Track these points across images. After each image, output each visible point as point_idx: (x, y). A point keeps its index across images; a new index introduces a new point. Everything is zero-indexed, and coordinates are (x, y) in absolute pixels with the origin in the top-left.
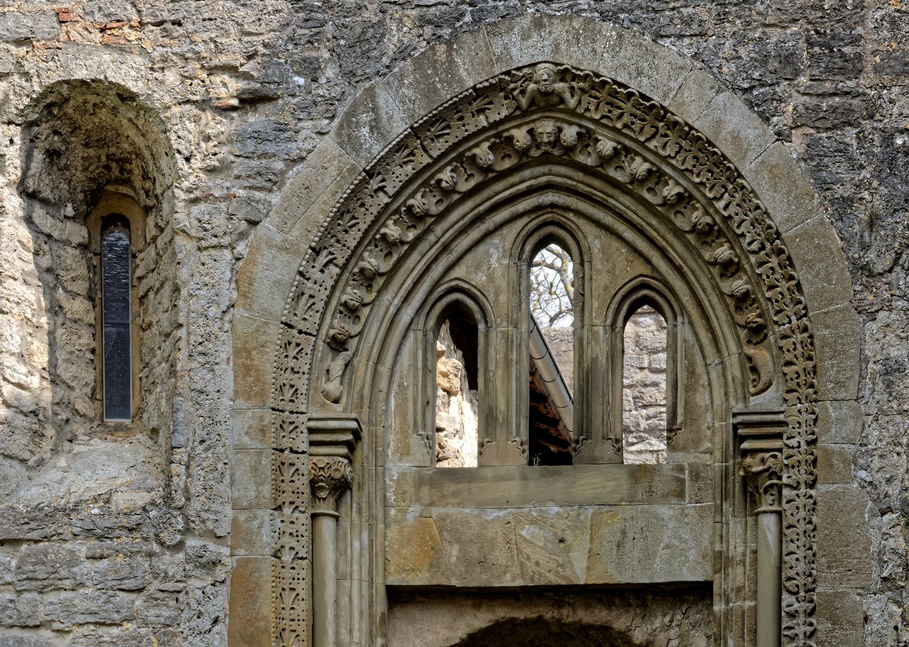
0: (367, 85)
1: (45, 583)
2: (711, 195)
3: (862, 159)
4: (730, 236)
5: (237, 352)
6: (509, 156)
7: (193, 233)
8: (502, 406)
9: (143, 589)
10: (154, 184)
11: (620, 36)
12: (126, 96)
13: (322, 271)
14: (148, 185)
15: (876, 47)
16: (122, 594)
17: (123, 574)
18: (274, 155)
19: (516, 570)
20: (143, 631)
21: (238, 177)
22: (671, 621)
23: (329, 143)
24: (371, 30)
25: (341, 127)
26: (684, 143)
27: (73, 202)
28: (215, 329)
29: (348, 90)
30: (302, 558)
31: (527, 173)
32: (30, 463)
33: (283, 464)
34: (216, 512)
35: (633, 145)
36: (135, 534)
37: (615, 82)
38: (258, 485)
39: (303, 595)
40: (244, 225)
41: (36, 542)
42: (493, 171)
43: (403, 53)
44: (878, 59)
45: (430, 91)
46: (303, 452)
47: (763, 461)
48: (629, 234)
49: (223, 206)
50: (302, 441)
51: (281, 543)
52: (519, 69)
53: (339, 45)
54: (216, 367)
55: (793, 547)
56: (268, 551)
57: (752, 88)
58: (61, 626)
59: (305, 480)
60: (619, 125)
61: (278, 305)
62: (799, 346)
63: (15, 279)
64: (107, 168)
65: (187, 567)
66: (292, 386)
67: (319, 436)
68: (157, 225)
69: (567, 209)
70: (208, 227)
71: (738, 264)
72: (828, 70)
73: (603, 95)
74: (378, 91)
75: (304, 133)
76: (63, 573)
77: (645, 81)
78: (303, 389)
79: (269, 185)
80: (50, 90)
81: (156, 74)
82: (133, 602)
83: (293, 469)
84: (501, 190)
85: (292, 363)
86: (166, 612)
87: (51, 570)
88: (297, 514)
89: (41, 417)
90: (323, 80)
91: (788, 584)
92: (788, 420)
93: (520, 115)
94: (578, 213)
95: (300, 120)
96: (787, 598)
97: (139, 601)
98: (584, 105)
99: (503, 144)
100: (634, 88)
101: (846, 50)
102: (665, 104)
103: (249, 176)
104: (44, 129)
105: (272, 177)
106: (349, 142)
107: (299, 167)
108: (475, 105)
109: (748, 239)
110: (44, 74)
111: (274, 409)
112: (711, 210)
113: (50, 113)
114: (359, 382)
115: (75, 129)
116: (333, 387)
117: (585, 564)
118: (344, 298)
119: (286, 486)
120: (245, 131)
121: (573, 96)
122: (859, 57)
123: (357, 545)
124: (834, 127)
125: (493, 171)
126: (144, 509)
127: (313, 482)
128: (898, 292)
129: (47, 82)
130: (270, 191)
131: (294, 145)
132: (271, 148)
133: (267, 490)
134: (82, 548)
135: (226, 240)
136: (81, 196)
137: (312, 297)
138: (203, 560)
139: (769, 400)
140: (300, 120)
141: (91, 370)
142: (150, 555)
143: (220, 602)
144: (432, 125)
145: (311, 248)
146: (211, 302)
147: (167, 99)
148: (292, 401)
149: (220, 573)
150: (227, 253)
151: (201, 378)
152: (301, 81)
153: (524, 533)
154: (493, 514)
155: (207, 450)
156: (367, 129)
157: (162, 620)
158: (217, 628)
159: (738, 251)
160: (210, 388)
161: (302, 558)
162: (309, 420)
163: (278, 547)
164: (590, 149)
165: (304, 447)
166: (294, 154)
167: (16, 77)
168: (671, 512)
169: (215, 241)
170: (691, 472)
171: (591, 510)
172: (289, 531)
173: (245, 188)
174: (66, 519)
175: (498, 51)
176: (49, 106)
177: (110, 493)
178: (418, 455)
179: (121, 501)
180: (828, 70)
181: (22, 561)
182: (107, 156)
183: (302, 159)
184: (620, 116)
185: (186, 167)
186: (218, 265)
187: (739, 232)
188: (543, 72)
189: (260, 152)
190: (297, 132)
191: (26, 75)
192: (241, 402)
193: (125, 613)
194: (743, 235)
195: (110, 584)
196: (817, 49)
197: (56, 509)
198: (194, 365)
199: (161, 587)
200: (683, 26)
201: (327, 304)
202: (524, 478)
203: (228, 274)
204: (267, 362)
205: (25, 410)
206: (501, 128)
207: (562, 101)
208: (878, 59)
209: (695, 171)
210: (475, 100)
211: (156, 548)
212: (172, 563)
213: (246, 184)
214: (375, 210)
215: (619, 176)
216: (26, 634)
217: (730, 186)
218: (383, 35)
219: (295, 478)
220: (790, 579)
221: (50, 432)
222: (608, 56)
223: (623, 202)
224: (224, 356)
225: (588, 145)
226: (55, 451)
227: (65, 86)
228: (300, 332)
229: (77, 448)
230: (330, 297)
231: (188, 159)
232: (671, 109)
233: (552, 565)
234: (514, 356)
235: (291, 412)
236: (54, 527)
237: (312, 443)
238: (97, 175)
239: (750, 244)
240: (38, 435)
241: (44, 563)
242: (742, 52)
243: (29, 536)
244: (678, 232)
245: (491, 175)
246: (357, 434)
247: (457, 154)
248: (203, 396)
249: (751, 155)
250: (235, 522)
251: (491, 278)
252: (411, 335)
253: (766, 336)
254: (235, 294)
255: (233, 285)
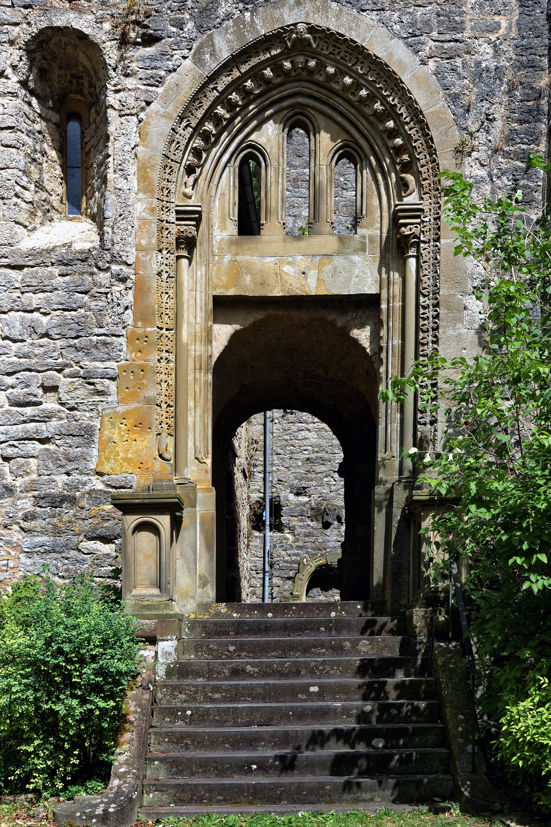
0: (209, 32)
1: (36, 288)
2: (385, 94)
3: (465, 74)
4: (394, 115)
5: (139, 169)
6: (280, 76)
7: (117, 107)
8: (273, 204)
9: (89, 291)
10: (95, 89)
11: (341, 10)
12: (82, 36)
13: (184, 130)
14: (92, 90)
15: (472, 17)
16: (77, 294)
17: (78, 283)
18: (160, 68)
19: (279, 288)
20: (88, 313)
21: (141, 79)
22: (356, 316)
23: (188, 63)
24: (211, 5)
25: (195, 54)
26: (372, 66)
27: (53, 99)
28: (128, 157)
29: (199, 35)
30: (172, 277)
31: (288, 86)
32: (29, 228)
33: (163, 228)
34: (127, 252)
35: (345, 69)
36: (84, 263)
37: (338, 33)
38: (149, 238)
39: (172, 296)
40: (144, 104)
41: (32, 267)
42: (271, 83)
43: (228, 16)
44: (473, 23)
45: (239, 34)
46: (173, 223)
47: (410, 229)
48: (339, 119)
49: (133, 93)
50: (172, 217)
51: (161, 268)
52: (288, 26)
53: (194, 12)
54: (128, 177)
55: (426, 272)
56: (155, 272)
57: (408, 38)
58: (45, 311)
59: (174, 237)
60: (338, 58)
61: (162, 147)
62: (430, 170)
63: (23, 133)
64: (70, 82)
65: (112, 280)
66: (167, 189)
67: (182, 215)
68: (96, 111)
69: (308, 106)
70: (125, 104)
71: (397, 130)
72: (448, 28)
73: (331, 41)
74: (214, 36)
75: (176, 57)
76: (46, 283)
77: (353, 33)
78: (173, 190)
79: (157, 83)
80: (42, 32)
81: (98, 25)
82: (83, 298)
83: (167, 232)
84: (275, 95)
85: (167, 176)
86: (101, 304)
87: (40, 281)
88: (169, 255)
89: (35, 205)
90: (186, 30)
91: (423, 291)
92: (424, 208)
93: (286, 54)
94: (314, 108)
95: (174, 50)
96: (422, 299)
97: (86, 298)
98: (321, 47)
99: (277, 69)
100: (348, 36)
101: (457, 18)
102: (364, 45)
103: (146, 79)
104: (38, 55)
105: (159, 79)
106: (198, 60)
107: (173, 74)
108: (265, 46)
109: (404, 116)
110: (38, 25)
111: (158, 199)
112: (384, 102)
113: (42, 46)
114: (201, 190)
115: (55, 57)
116: (188, 190)
117: (315, 285)
118: (194, 145)
119: (164, 240)
120: (144, 55)
121: (315, 42)
122: (462, 22)
123: (201, 272)
124: (451, 58)
125: (271, 83)
126: (89, 250)
127: (177, 239)
128: (482, 142)
129: (40, 27)
130: (157, 86)
131: (170, 63)
132: (158, 64)
133: (154, 241)
134: (56, 270)
135: (134, 111)
136: (56, 97)
137: (178, 143)
138: (121, 276)
139: (412, 199)
140: (174, 50)
141: (61, 188)
142: (92, 274)
143: (129, 298)
144: (242, 55)
145: (178, 116)
146: (126, 143)
147: (104, 38)
148: (167, 196)
149: (129, 284)
150: (135, 119)
151: (122, 184)
152: (174, 30)
153: (284, 269)
154: (268, 260)
155: (123, 219)
156: (209, 55)
157: (98, 307)
158: (127, 312)
159: (398, 123)
160: (126, 188)
161: (172, 277)
162: (177, 206)
163: (160, 270)
164: (322, 72)
165: (174, 220)
166: (171, 67)
167: (25, 26)
168: (359, 259)
169: (128, 112)
170: (369, 239)
171: (318, 258)
172: (165, 262)
173: (144, 85)
174: (48, 255)
175: (277, 16)
176: (42, 41)
177: (71, 243)
178: (231, 230)
179: (78, 246)
180: (448, 28)
181: (25, 276)
182: (71, 75)
183: (175, 70)
184: (339, 53)
185: (113, 73)
186: (129, 124)
187: (400, 112)
188: (301, 27)
189: (152, 66)
190: (172, 56)
191: (29, 24)
192: (141, 195)
193: (79, 304)
194: (402, 114)
195: (71, 289)
196: (442, 18)
197: (43, 250)
198: (117, 175)
199: (98, 290)
200: (373, 5)
201: (186, 148)
202: (285, 241)
203: (135, 129)
204: (155, 175)
205: (27, 200)
206: (277, 59)
207: (310, 45)
208: (473, 23)
209: (378, 81)
210: (264, 43)
211: (95, 270)
212: (103, 277)
213: (145, 82)
214: (212, 99)
215: (337, 87)
216: (26, 314)
217: (396, 89)
218: (217, 7)
219: (169, 236)
220: (424, 289)
221: (40, 214)
222: (338, 21)
223: (338, 102)
224: (132, 171)
225: (320, 71)
226: (42, 224)
227: (50, 30)
228: (172, 160)
229: (53, 224)
230: (188, 144)
231: (114, 70)
232: (366, 47)
233: (298, 285)
234: (280, 180)
235: (167, 202)
236: (41, 259)
237: (177, 219)
238: (67, 84)
239: (405, 119)
240: (33, 214)
241: (36, 278)
242: (404, 19)
243: (28, 263)
244: (365, 117)
245: (271, 85)
246: (199, 213)
247: (255, 74)
248: (121, 192)
249: (408, 72)
250: (137, 258)
251: (269, 140)
252: (227, 169)
253: (411, 167)
254: (138, 140)
255: (138, 135)
